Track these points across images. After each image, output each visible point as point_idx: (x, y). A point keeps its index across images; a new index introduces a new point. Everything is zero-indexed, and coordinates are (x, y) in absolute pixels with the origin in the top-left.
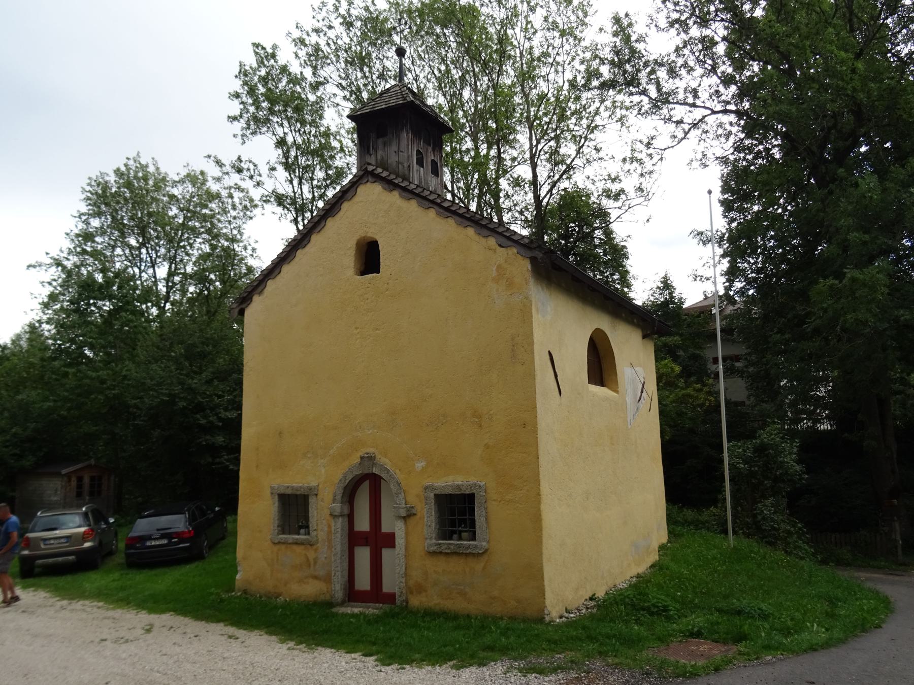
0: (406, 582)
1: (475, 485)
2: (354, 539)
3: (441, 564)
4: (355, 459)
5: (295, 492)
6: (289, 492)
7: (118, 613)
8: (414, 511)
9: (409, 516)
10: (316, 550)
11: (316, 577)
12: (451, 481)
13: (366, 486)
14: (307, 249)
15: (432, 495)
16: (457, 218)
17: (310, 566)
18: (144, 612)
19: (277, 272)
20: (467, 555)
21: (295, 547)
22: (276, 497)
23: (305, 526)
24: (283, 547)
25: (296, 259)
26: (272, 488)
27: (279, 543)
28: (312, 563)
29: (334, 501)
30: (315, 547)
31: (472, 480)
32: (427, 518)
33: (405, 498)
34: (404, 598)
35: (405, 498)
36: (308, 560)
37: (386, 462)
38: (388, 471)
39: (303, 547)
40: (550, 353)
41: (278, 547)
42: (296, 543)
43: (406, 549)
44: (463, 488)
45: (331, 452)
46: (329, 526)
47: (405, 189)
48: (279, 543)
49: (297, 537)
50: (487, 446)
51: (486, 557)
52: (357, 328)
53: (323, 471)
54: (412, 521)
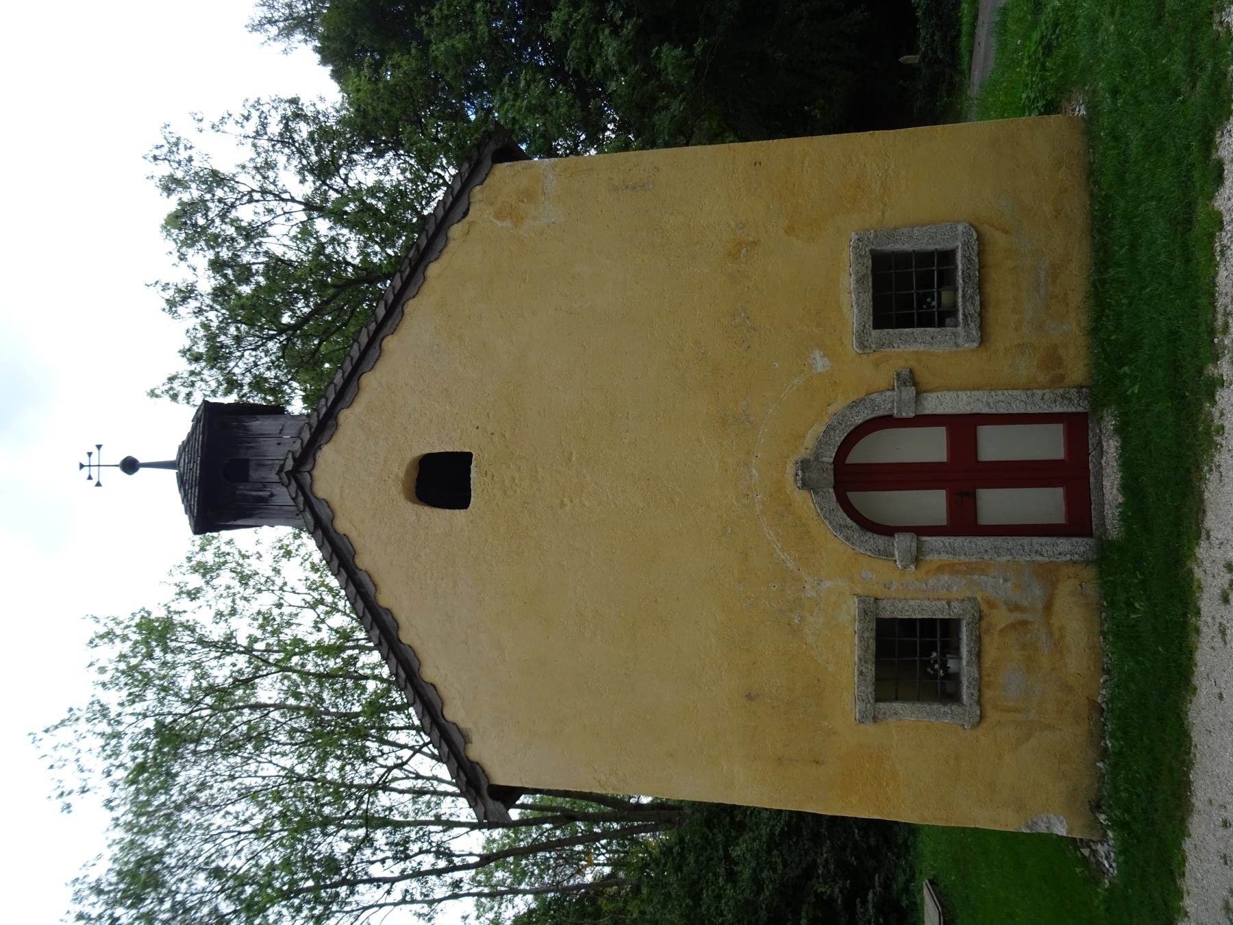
0: (1043, 388)
1: (856, 248)
4: (803, 501)
8: (905, 372)
10: (992, 605)
11: (1048, 608)
12: (850, 301)
14: (402, 618)
15: (875, 333)
16: (409, 293)
17: (1025, 623)
19: (431, 693)
20: (982, 266)
21: (987, 662)
22: (881, 705)
24: (988, 694)
27: (979, 702)
28: (1019, 616)
30: (984, 607)
31: (848, 255)
32: (913, 346)
36: (1013, 626)
37: (812, 433)
41: (988, 708)
42: (978, 655)
43: (978, 389)
45: (791, 565)
46: (940, 569)
48: (979, 702)
50: (790, 230)
51: (985, 228)
52: (562, 505)
53: (828, 584)
54: (924, 377)
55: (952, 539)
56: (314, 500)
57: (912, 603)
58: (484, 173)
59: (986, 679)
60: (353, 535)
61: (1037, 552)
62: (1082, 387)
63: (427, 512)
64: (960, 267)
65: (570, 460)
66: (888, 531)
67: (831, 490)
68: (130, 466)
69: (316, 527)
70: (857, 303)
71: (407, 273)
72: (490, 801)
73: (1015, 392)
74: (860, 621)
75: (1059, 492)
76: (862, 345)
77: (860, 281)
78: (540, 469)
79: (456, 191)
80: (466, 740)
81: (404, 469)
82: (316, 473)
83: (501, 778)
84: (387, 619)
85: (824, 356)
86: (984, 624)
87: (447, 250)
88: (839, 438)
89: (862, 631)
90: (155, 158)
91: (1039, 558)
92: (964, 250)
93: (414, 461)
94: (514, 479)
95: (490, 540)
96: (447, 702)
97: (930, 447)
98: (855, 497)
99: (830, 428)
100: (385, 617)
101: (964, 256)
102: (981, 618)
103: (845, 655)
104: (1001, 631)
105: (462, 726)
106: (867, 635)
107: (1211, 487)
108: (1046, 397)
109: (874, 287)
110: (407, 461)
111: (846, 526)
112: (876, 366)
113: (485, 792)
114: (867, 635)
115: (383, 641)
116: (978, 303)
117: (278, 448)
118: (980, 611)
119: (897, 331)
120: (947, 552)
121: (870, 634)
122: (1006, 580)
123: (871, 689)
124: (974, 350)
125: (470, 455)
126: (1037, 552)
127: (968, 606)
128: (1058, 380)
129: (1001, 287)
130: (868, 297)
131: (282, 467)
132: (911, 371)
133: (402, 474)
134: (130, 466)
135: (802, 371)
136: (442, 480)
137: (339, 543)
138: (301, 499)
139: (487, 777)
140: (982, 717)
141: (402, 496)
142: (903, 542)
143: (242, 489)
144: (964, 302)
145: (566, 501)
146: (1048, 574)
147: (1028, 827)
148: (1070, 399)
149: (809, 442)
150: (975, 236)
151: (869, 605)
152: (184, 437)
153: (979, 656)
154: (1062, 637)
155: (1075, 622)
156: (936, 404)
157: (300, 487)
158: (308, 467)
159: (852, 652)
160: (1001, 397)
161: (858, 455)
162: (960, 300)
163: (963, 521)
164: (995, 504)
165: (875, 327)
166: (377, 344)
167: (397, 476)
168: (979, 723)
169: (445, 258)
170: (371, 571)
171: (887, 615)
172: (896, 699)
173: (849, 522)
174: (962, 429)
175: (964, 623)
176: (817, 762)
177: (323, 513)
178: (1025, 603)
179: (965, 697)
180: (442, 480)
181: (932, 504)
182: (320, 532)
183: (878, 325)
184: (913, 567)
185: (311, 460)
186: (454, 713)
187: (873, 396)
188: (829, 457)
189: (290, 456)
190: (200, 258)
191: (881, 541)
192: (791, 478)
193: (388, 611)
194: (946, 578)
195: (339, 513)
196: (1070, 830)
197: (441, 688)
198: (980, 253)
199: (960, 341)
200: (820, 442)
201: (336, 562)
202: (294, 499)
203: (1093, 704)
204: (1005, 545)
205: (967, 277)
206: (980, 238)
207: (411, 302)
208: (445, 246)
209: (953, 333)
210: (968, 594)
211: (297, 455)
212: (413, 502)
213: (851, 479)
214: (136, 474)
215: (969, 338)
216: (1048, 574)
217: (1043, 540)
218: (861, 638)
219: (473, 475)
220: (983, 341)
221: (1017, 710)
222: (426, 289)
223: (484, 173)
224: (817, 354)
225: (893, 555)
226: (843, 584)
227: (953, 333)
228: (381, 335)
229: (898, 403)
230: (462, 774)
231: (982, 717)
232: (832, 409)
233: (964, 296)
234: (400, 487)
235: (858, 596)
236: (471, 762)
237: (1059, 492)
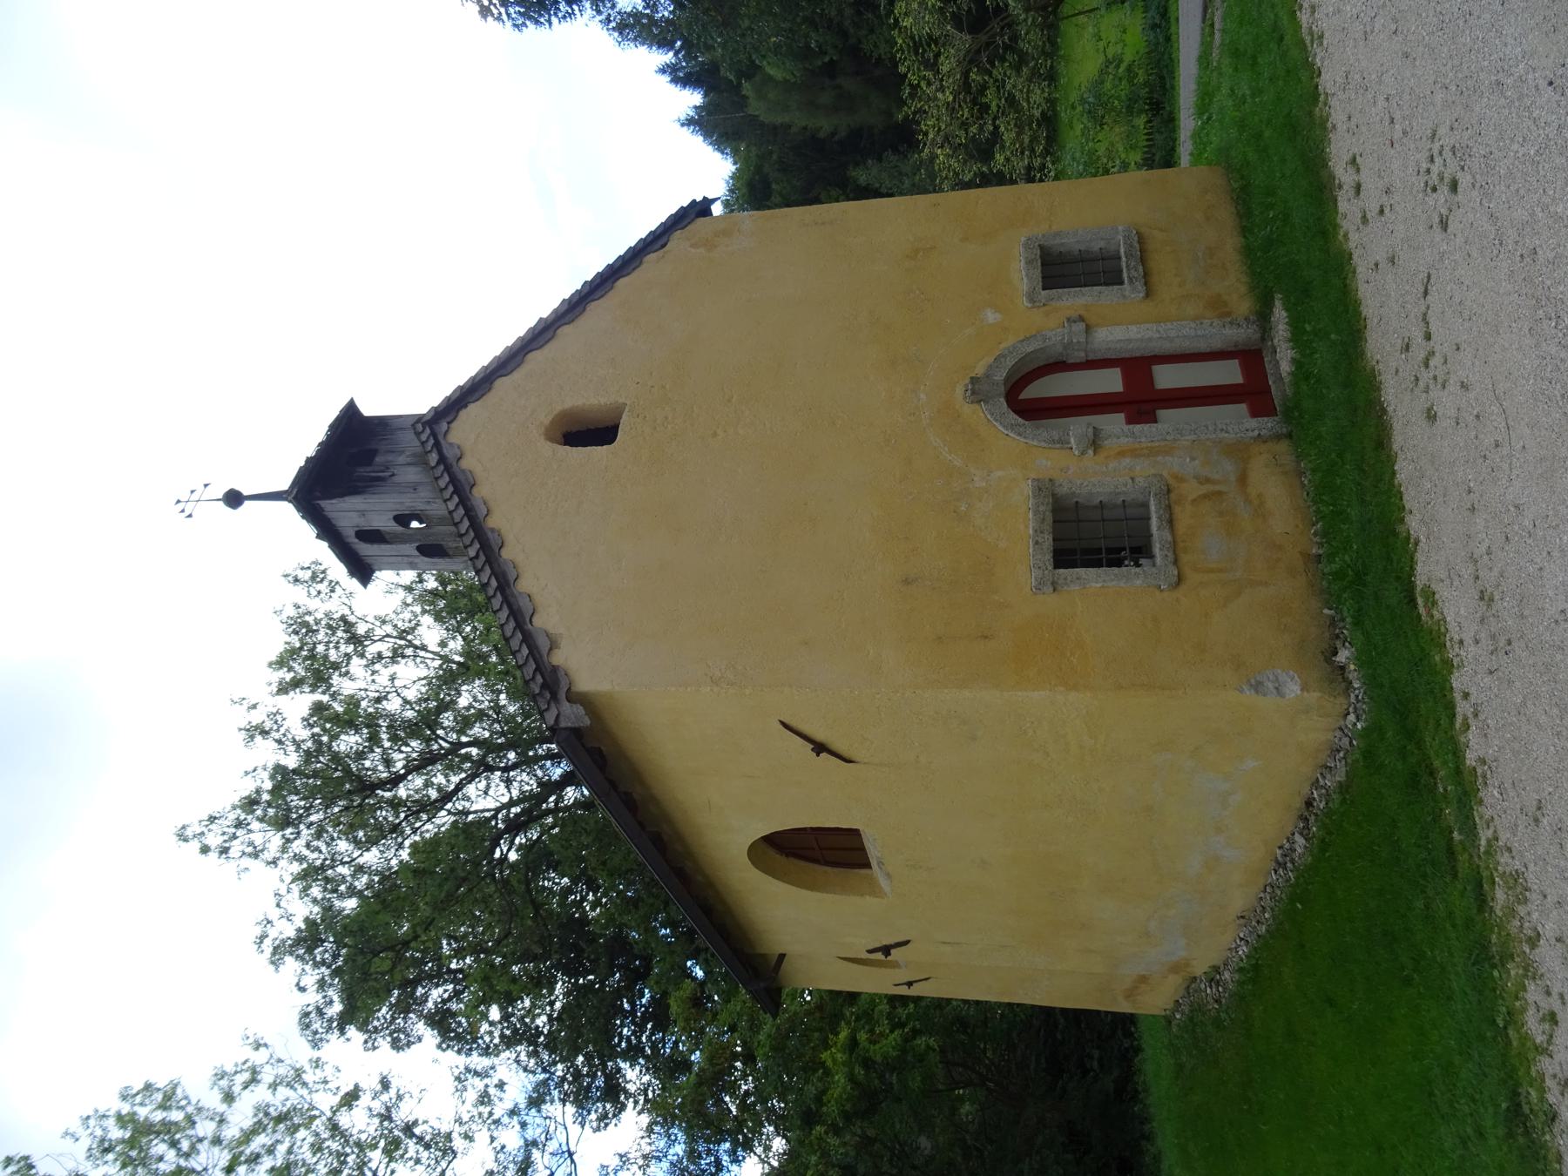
2: (1137, 367)
4: (975, 414)
5: (1048, 526)
6: (1048, 541)
7: (1456, 610)
11: (1243, 480)
12: (1021, 275)
13: (1034, 391)
17: (1220, 493)
22: (1062, 571)
24: (1185, 558)
27: (1176, 562)
29: (1063, 443)
30: (1171, 482)
36: (1205, 497)
39: (1177, 509)
40: (907, 942)
46: (1121, 454)
47: (520, 626)
49: (1154, 522)
52: (715, 435)
53: (1000, 473)
59: (1181, 545)
68: (234, 499)
76: (1032, 300)
77: (1029, 262)
81: (550, 418)
86: (1173, 496)
90: (296, 580)
102: (1169, 491)
103: (1019, 535)
104: (1194, 501)
106: (1042, 508)
107: (1354, 238)
110: (558, 408)
113: (562, 695)
114: (1042, 508)
122: (1193, 459)
134: (234, 499)
143: (363, 471)
146: (1238, 451)
151: (1045, 488)
152: (310, 450)
153: (1171, 522)
155: (1276, 495)
159: (1027, 527)
184: (1091, 452)
190: (299, 704)
194: (1127, 461)
203: (1306, 556)
210: (1153, 471)
214: (241, 509)
216: (1238, 451)
218: (1036, 513)
220: (1148, 294)
221: (1220, 571)
226: (1016, 472)
231: (1180, 580)
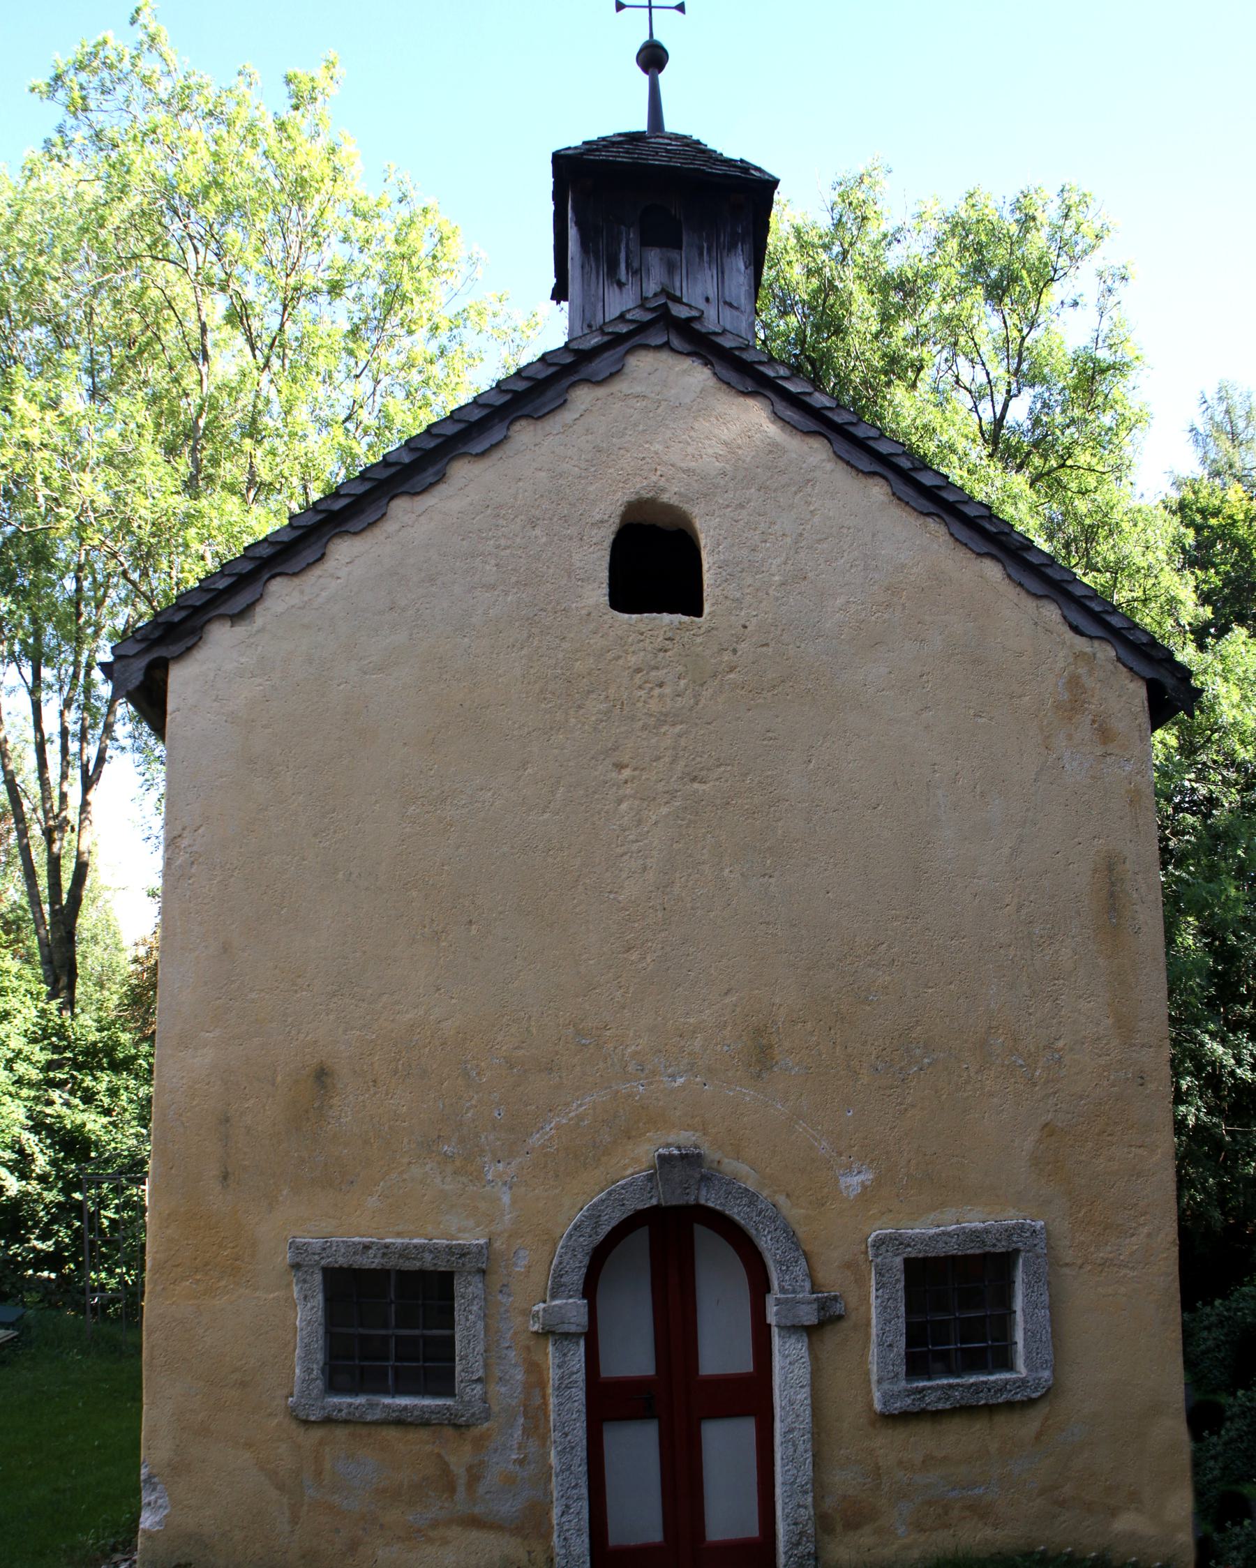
0: (816, 1504)
1: (1022, 1227)
3: (922, 1441)
4: (640, 1156)
5: (393, 1263)
8: (839, 1308)
9: (825, 1323)
10: (479, 1443)
14: (428, 501)
15: (898, 1261)
16: (957, 527)
17: (451, 1488)
18: (517, 427)
19: (309, 555)
20: (991, 1409)
21: (391, 1433)
22: (318, 1277)
23: (431, 1366)
24: (341, 1433)
25: (389, 526)
26: (297, 1248)
27: (328, 1421)
28: (462, 1481)
30: (475, 1431)
31: (1011, 1218)
32: (879, 1314)
33: (811, 1275)
34: (811, 1547)
35: (811, 1275)
36: (446, 1470)
37: (751, 1174)
38: (752, 1198)
39: (424, 1434)
41: (317, 1434)
42: (400, 1421)
43: (814, 1414)
44: (990, 1240)
45: (535, 1140)
48: (328, 1421)
50: (1048, 1130)
51: (1043, 1409)
52: (620, 767)
53: (506, 1199)
54: (832, 1338)
55: (582, 1384)
56: (621, 349)
57: (480, 1325)
58: (1134, 664)
60: (566, 416)
61: (568, 1506)
62: (816, 1559)
63: (607, 535)
64: (992, 1378)
65: (694, 779)
66: (590, 1290)
67: (654, 1202)
69: (577, 352)
70: (944, 1233)
71: (988, 526)
72: (143, 662)
73: (808, 1466)
74: (450, 1247)
75: (655, 1534)
76: (880, 1243)
77: (975, 1235)
78: (678, 728)
79: (1108, 618)
80: (238, 617)
81: (674, 501)
82: (665, 357)
83: (184, 682)
84: (428, 476)
85: (865, 1187)
86: (449, 1432)
87: (1023, 594)
88: (736, 1212)
89: (435, 1250)
91: (556, 1512)
92: (1015, 1381)
93: (690, 524)
94: (661, 685)
95: (565, 645)
96: (296, 581)
97: (721, 1351)
98: (641, 1238)
99: (752, 1198)
100: (431, 471)
101: (1007, 1382)
102: (457, 1427)
104: (439, 1456)
105: (259, 609)
106: (428, 1257)
108: (802, 1511)
109: (966, 1257)
111: (597, 1224)
112: (848, 1265)
115: (393, 470)
116: (940, 1406)
117: (702, 292)
118: (468, 1426)
119: (901, 1294)
120: (561, 1378)
121: (428, 1262)
123: (342, 1261)
124: (870, 1404)
125: (699, 614)
126: (568, 1506)
127: (477, 1408)
128: (824, 1522)
129: (958, 1439)
130: (953, 1249)
131: (678, 300)
132: (840, 1318)
133: (665, 498)
135: (840, 1154)
136: (655, 563)
137: (550, 393)
138: (623, 329)
139: (179, 657)
140: (306, 1423)
141: (633, 497)
142: (573, 1309)
144: (942, 1387)
145: (626, 773)
147: (150, 1477)
148: (798, 1543)
149: (732, 1166)
150: (1034, 1395)
154: (430, 1541)
156: (789, 1360)
157: (642, 327)
158: (676, 342)
159: (399, 1235)
160: (801, 1448)
161: (705, 1239)
162: (945, 1381)
163: (608, 1402)
164: (636, 1448)
165: (908, 1262)
166: (878, 469)
167: (663, 490)
168: (296, 1418)
169: (1011, 592)
170: (509, 448)
171: (459, 1288)
172: (327, 1300)
173: (605, 1229)
174: (750, 1396)
175: (449, 1402)
176: (225, 1177)
177: (600, 366)
178: (481, 1490)
179: (336, 1400)
180: (655, 563)
181: (632, 1355)
182: (568, 359)
183: (911, 1265)
185: (687, 348)
186: (282, 595)
187: (803, 1261)
188: (711, 1199)
189: (695, 313)
191: (576, 1278)
192: (672, 1138)
193: (441, 478)
195: (601, 392)
196: (150, 1536)
197: (317, 571)
198: (1010, 1406)
199: (886, 1386)
200: (730, 1183)
201: (521, 386)
202: (622, 317)
204: (577, 1461)
205: (977, 1388)
206: (1031, 1402)
207: (942, 530)
208: (1028, 592)
209: (896, 1375)
211: (697, 326)
212: (624, 516)
213: (672, 1238)
215: (887, 1398)
217: (585, 1514)
218: (420, 1249)
219: (666, 617)
222: (962, 555)
223: (1134, 664)
224: (867, 1177)
225: (553, 1297)
227: (896, 1375)
228: (890, 476)
229: (787, 1293)
230: (183, 614)
231: (306, 1423)
232: (781, 1199)
233: (951, 1386)
234: (646, 495)
235: (489, 1244)
236: (202, 628)
237: (655, 1534)
